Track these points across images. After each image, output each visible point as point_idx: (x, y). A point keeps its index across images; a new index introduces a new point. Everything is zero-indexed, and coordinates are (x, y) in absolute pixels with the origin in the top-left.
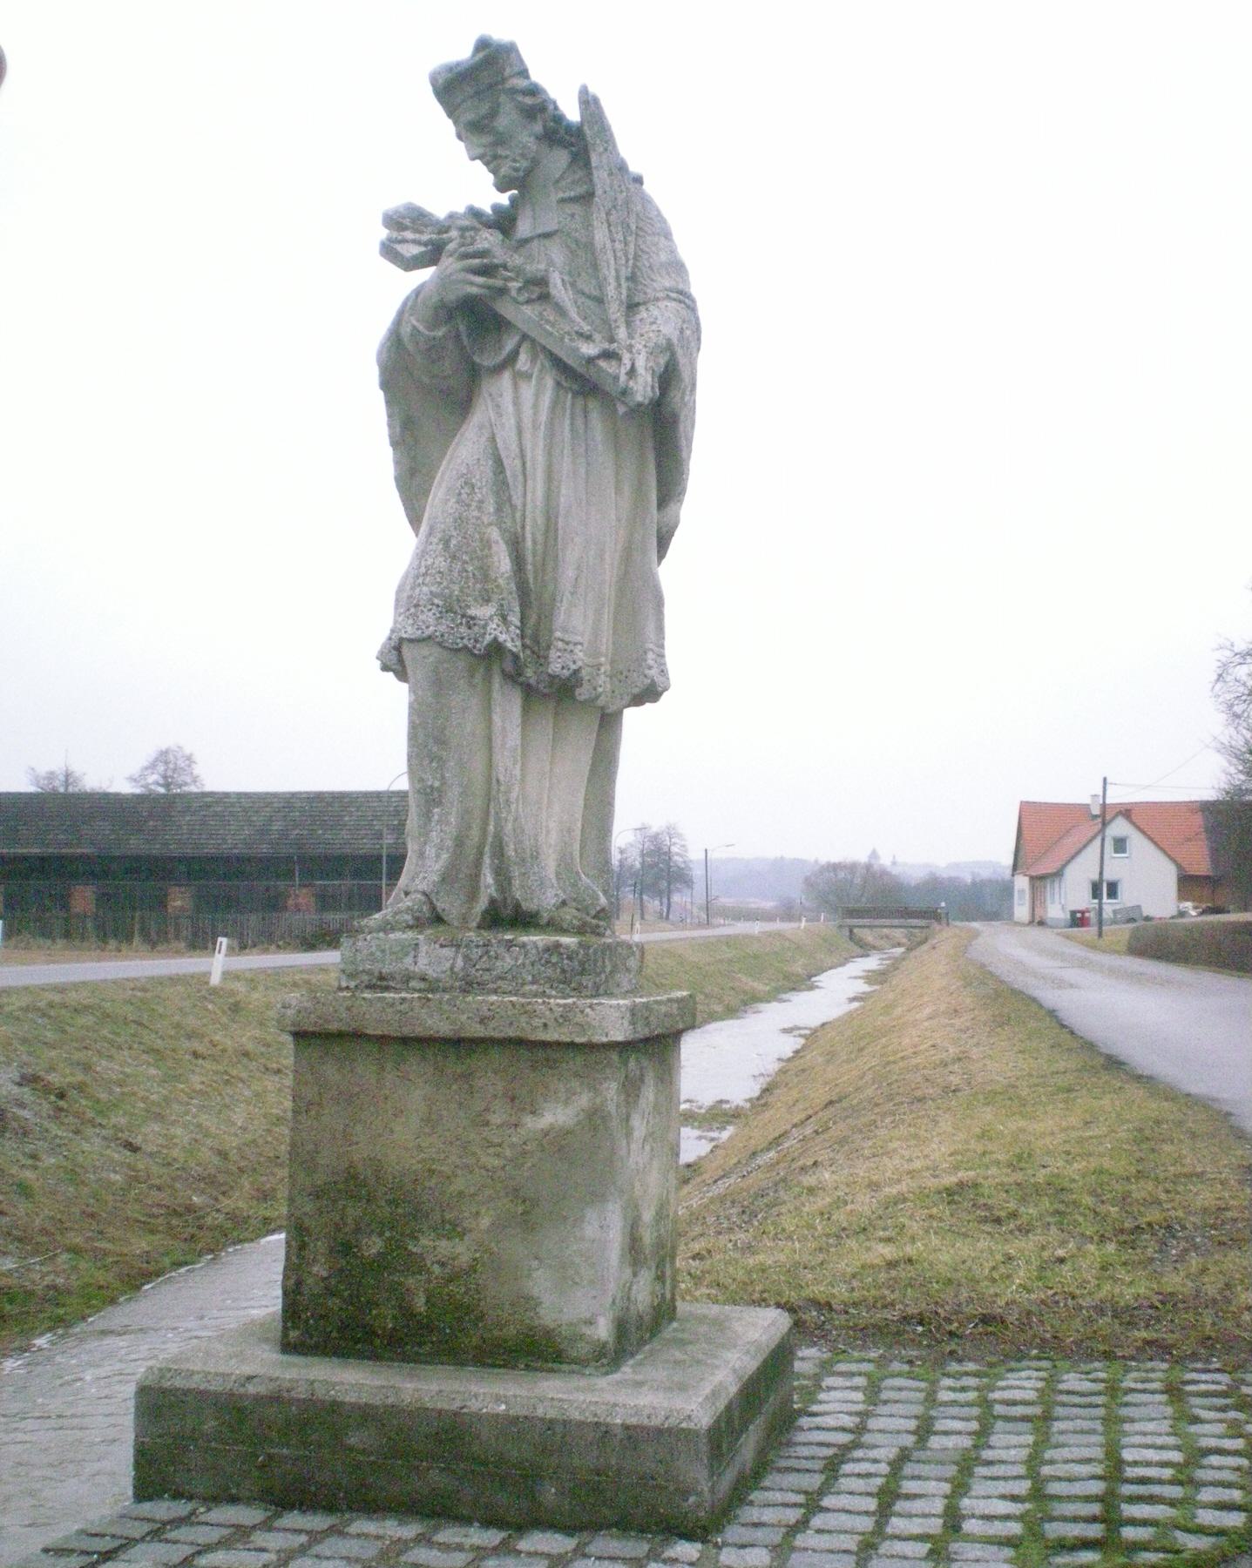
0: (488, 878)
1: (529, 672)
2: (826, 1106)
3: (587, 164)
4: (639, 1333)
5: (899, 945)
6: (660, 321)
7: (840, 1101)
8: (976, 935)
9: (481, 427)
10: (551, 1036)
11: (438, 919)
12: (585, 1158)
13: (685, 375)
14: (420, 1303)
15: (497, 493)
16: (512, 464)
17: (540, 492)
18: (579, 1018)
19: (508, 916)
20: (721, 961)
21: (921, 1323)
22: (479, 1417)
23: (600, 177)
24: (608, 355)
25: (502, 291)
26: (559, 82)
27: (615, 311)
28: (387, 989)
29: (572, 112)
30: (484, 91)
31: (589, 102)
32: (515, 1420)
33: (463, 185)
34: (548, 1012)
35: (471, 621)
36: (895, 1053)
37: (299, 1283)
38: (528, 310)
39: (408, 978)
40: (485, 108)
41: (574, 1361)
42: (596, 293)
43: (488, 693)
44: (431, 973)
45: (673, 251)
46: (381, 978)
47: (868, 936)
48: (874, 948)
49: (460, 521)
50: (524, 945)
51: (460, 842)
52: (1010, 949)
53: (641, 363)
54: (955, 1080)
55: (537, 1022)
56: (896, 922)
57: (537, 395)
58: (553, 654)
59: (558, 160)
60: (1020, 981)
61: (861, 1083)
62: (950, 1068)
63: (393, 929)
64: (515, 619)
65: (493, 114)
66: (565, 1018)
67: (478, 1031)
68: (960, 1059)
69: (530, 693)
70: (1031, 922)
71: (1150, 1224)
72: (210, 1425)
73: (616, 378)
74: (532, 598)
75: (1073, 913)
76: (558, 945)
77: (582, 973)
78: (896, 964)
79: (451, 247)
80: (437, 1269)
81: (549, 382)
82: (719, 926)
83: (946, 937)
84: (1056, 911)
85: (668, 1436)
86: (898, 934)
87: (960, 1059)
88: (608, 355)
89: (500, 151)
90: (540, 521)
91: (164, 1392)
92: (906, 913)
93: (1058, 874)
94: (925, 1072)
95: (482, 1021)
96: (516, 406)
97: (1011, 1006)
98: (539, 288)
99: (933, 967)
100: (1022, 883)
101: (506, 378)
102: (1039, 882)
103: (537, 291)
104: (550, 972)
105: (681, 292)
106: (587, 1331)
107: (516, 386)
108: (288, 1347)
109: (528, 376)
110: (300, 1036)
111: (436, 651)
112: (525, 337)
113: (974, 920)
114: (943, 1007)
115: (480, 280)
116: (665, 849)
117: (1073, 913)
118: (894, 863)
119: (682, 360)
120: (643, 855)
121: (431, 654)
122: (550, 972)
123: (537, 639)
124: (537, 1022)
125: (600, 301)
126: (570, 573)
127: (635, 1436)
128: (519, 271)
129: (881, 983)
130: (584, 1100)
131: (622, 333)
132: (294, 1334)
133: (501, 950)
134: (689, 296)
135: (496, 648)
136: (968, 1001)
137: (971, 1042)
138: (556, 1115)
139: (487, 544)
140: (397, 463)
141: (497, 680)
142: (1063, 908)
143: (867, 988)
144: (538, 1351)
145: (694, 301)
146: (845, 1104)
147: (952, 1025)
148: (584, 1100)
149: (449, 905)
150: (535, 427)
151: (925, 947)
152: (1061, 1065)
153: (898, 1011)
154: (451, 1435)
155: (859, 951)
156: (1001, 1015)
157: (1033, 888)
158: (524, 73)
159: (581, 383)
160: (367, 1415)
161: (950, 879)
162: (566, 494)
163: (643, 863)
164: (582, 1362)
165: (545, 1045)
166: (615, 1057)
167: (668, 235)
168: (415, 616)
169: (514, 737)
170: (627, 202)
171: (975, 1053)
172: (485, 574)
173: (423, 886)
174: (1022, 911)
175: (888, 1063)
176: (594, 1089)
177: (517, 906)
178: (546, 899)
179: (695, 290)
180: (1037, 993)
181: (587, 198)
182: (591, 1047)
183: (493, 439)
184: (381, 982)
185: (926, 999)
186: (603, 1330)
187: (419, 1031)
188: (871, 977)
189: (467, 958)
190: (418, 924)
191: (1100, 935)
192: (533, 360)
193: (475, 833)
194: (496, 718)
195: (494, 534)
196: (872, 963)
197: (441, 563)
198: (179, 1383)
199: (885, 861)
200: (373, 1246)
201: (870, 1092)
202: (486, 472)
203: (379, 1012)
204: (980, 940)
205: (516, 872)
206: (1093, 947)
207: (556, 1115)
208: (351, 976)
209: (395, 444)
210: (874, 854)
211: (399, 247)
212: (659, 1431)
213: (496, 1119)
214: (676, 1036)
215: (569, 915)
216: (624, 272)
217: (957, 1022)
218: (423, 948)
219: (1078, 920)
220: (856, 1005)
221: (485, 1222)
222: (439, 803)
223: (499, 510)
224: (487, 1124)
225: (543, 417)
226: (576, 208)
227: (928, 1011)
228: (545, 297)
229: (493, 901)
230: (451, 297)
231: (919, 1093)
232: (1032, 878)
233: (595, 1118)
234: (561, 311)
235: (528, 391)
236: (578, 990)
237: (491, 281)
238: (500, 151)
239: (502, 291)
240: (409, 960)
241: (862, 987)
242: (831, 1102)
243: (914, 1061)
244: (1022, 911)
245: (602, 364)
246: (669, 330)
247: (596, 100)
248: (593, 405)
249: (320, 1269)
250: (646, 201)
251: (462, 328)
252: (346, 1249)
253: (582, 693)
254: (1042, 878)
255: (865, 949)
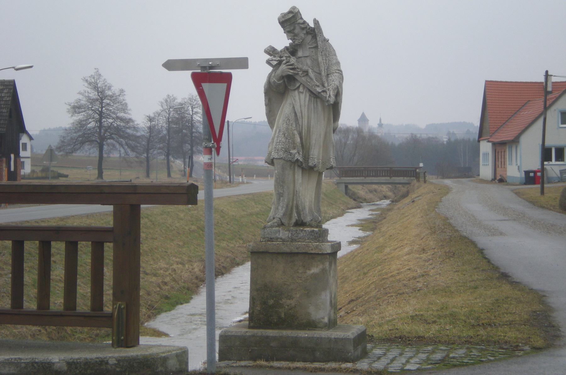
0: (295, 215)
1: (304, 165)
2: (349, 303)
3: (316, 39)
4: (332, 324)
5: (386, 197)
6: (334, 77)
7: (357, 299)
8: (448, 190)
9: (290, 104)
10: (313, 252)
11: (282, 224)
12: (321, 281)
13: (340, 92)
14: (283, 316)
15: (296, 122)
16: (299, 115)
17: (306, 121)
18: (320, 248)
19: (300, 224)
20: (251, 214)
21: (400, 338)
22: (301, 337)
23: (320, 43)
24: (323, 91)
25: (298, 74)
26: (308, 18)
27: (324, 79)
28: (273, 241)
29: (312, 25)
30: (290, 21)
31: (316, 22)
32: (309, 338)
33: (282, 41)
34: (313, 246)
35: (291, 154)
36: (387, 274)
37: (253, 312)
38: (303, 78)
39: (277, 238)
40: (292, 28)
41: (320, 328)
42: (318, 72)
43: (294, 169)
44: (283, 237)
45: (337, 59)
46: (271, 239)
47: (361, 191)
48: (365, 200)
49: (287, 129)
50: (305, 231)
51: (287, 206)
52: (469, 203)
53: (331, 94)
54: (420, 285)
55: (310, 249)
56: (383, 179)
57: (305, 98)
58: (310, 161)
59: (309, 37)
60: (467, 230)
61: (368, 290)
62: (417, 280)
63: (273, 227)
64: (301, 153)
65: (294, 29)
66: (317, 247)
67: (296, 251)
68: (423, 276)
69: (303, 169)
70: (494, 179)
71: (483, 324)
72: (237, 343)
73: (326, 97)
74: (305, 147)
75: (527, 173)
76: (313, 231)
77: (320, 237)
78: (383, 214)
79: (284, 62)
80: (286, 307)
81: (308, 95)
82: (239, 183)
83: (422, 192)
84: (513, 171)
85: (344, 340)
86: (385, 189)
87: (423, 276)
88: (323, 91)
89: (296, 38)
90: (306, 129)
91: (226, 336)
92: (392, 172)
93: (516, 141)
94: (404, 282)
95: (297, 248)
96: (298, 100)
97: (459, 245)
98: (306, 73)
99: (411, 218)
100: (486, 147)
101: (296, 92)
102: (500, 147)
103: (305, 74)
104: (312, 237)
105: (339, 70)
106: (322, 320)
107: (299, 95)
108: (250, 327)
109: (302, 93)
110: (252, 253)
111: (283, 161)
112: (301, 84)
113: (449, 177)
114: (416, 247)
115: (292, 71)
116: (188, 117)
117: (527, 173)
118: (380, 125)
119: (340, 90)
120: (169, 122)
121: (282, 162)
122: (312, 237)
123: (306, 157)
124: (310, 249)
125: (320, 74)
126: (314, 142)
127: (337, 340)
128: (301, 69)
129: (373, 229)
130: (321, 266)
131: (326, 85)
132: (252, 324)
133: (300, 232)
134: (341, 71)
135: (297, 160)
136: (432, 243)
137: (431, 267)
138: (314, 270)
139: (294, 135)
140: (266, 110)
141: (296, 167)
142: (519, 168)
143: (361, 234)
144: (311, 325)
145: (342, 72)
146: (360, 300)
147: (421, 258)
148: (321, 266)
149: (285, 221)
150: (305, 106)
151: (407, 200)
152: (475, 277)
153: (387, 250)
154: (295, 342)
155: (352, 202)
156: (449, 252)
157: (495, 152)
158: (302, 18)
159: (315, 96)
160: (275, 338)
161: (429, 139)
162: (313, 122)
163: (169, 130)
164: (322, 328)
165: (311, 254)
166: (328, 256)
167: (335, 55)
168: (278, 153)
169: (300, 181)
170: (326, 49)
171: (432, 272)
172: (294, 142)
173: (279, 216)
174: (486, 170)
175: (383, 279)
176: (100, 331)
177: (302, 221)
178: (308, 219)
179: (342, 68)
180: (475, 239)
181: (316, 47)
182: (323, 254)
183: (294, 107)
184: (271, 240)
185: (406, 242)
186: (326, 320)
187: (282, 251)
188: (363, 225)
189: (292, 234)
190: (278, 226)
191: (542, 192)
192: (304, 89)
193: (291, 203)
194: (296, 176)
195: (296, 132)
196: (363, 213)
197: (283, 140)
198: (229, 334)
199: (373, 123)
200: (271, 302)
201: (374, 293)
202: (292, 117)
203: (272, 246)
204: (450, 196)
205: (302, 213)
206: (534, 203)
207: (314, 270)
208: (264, 238)
209: (266, 105)
210: (363, 119)
211: (271, 62)
212: (342, 339)
213: (300, 271)
214: (337, 252)
215: (314, 223)
216: (326, 68)
217: (424, 256)
218: (281, 232)
219: (532, 178)
220: (355, 246)
221: (298, 296)
222: (282, 196)
223: (296, 126)
224: (298, 272)
225: (307, 103)
226: (313, 50)
227: (406, 250)
228: (307, 75)
229: (297, 220)
230: (284, 74)
231: (401, 292)
232: (494, 144)
233: (324, 271)
234: (311, 79)
235: (302, 96)
236: (319, 241)
237: (295, 72)
238: (296, 38)
239: (298, 74)
240: (277, 235)
241: (358, 233)
242: (352, 300)
243: (398, 277)
244: (486, 170)
245: (322, 94)
246: (337, 83)
247: (318, 22)
248: (318, 100)
249: (258, 308)
250: (330, 46)
251: (286, 80)
252: (265, 303)
253: (315, 169)
254: (503, 144)
255: (358, 202)
